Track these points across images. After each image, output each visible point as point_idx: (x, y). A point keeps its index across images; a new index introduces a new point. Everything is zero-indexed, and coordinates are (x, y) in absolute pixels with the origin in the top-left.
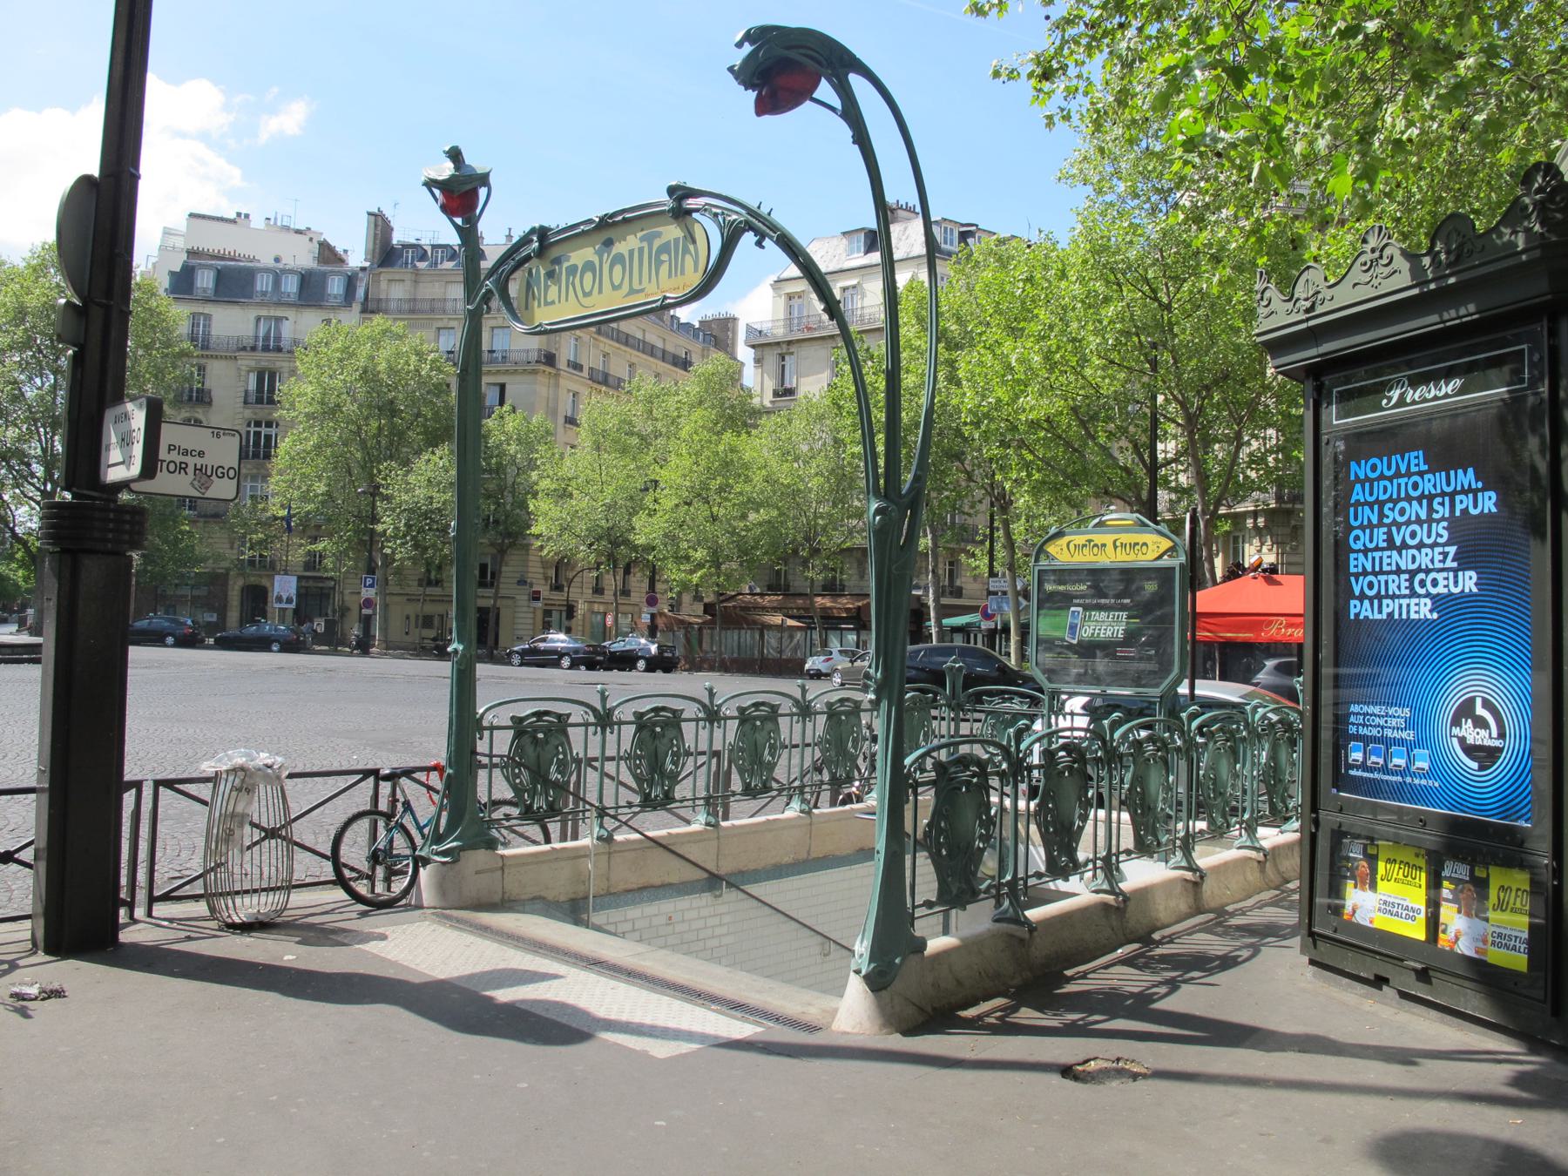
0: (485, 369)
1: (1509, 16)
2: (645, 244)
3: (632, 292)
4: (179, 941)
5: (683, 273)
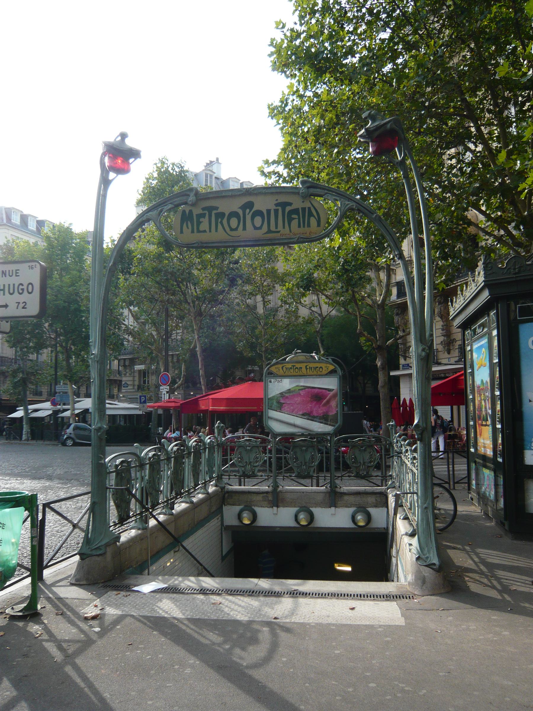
2: (280, 208)
5: (309, 226)
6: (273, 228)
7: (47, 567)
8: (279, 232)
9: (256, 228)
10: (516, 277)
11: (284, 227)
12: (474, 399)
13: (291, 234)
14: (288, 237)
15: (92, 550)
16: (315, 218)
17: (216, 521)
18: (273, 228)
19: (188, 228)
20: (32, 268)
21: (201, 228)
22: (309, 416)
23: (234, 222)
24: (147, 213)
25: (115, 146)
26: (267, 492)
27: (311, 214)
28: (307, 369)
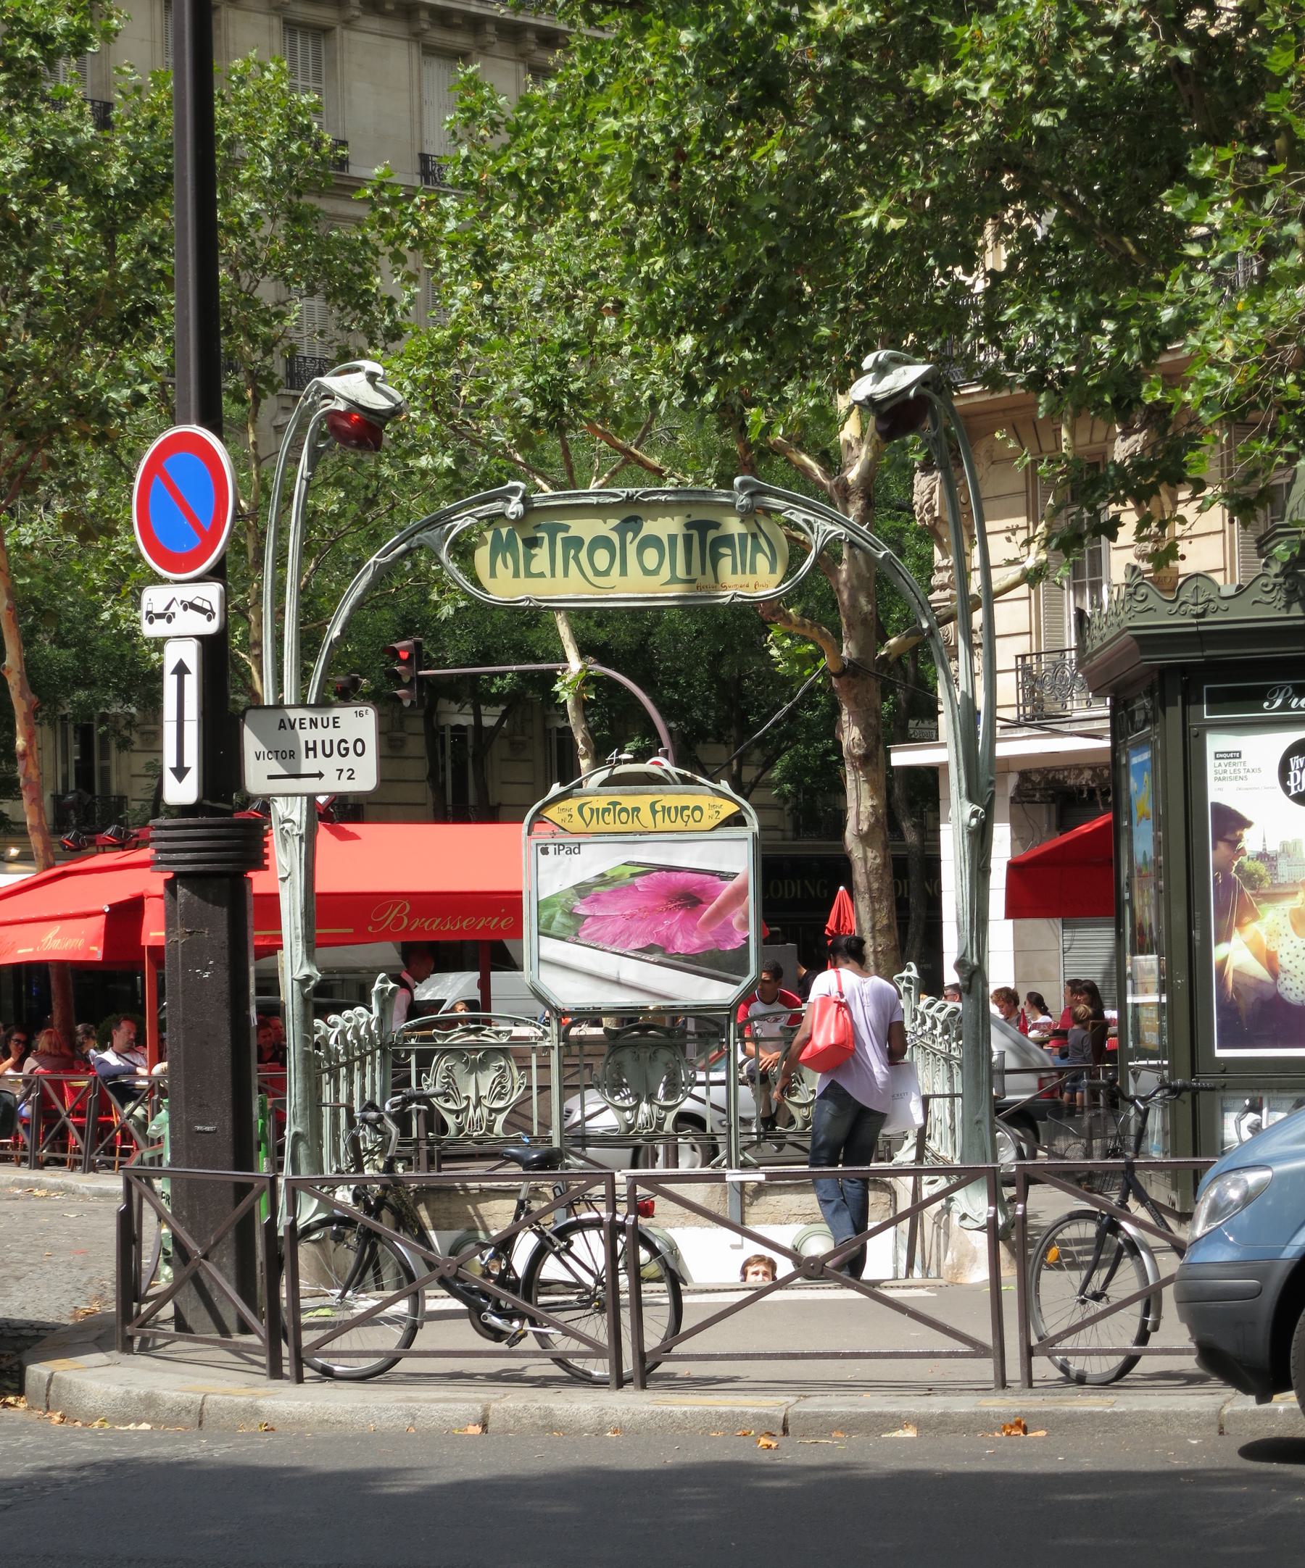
0: (1107, 724)
1: (924, 119)
2: (695, 533)
5: (753, 570)
11: (703, 573)
12: (1131, 901)
20: (361, 715)
21: (534, 569)
22: (659, 951)
23: (602, 557)
28: (654, 812)
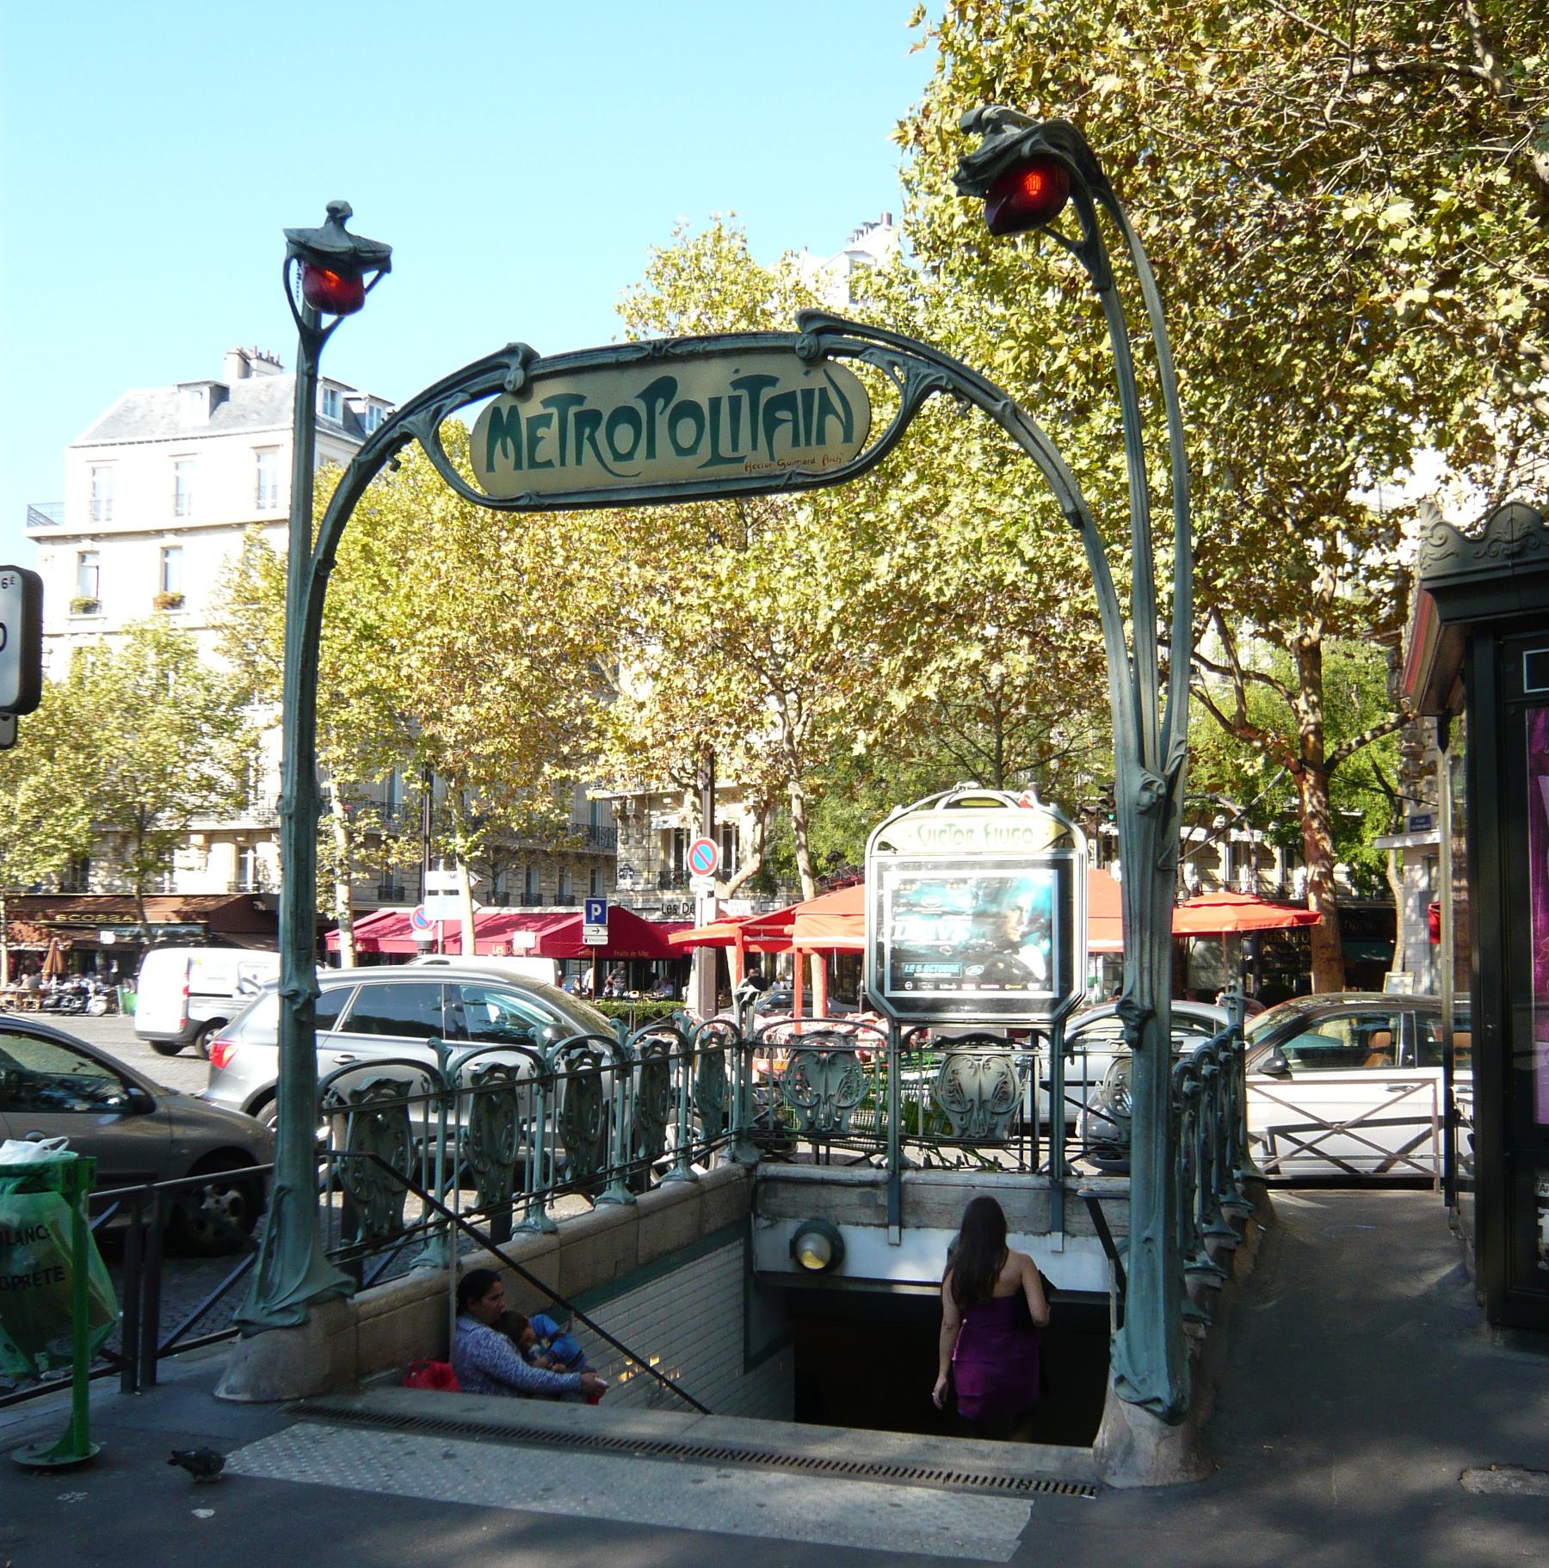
2: (744, 394)
3: (716, 459)
4: (785, 1486)
5: (821, 439)
6: (725, 449)
7: (168, 1351)
8: (740, 460)
9: (681, 451)
10: (1514, 566)
11: (755, 447)
13: (774, 465)
14: (765, 471)
15: (271, 1314)
16: (838, 416)
17: (734, 1255)
18: (725, 449)
19: (506, 455)
23: (624, 435)
24: (403, 418)
25: (312, 244)
26: (873, 1184)
27: (826, 408)
